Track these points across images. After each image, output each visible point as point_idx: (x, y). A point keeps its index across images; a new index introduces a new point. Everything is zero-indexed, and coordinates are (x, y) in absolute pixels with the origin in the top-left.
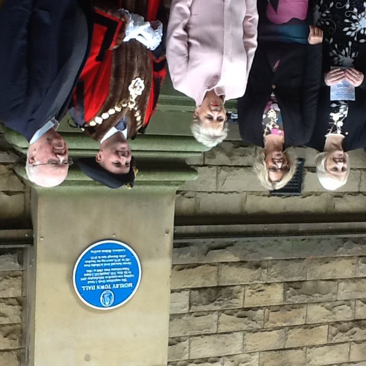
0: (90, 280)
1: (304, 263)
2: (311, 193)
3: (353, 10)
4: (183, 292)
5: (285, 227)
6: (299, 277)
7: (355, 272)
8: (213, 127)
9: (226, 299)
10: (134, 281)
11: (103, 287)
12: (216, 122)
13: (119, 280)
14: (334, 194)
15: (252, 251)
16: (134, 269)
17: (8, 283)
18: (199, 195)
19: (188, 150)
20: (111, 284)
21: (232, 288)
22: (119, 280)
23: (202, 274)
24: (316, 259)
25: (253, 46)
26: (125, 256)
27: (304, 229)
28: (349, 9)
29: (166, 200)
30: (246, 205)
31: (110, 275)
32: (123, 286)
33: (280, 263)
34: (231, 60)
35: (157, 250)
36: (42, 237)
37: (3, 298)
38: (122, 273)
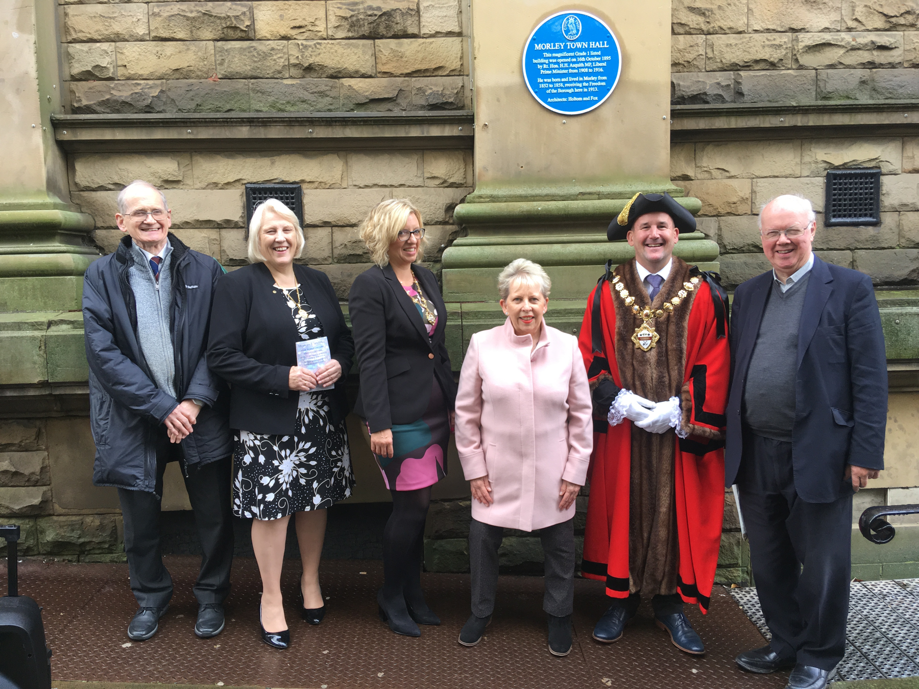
0: (598, 56)
1: (221, 71)
2: (226, 187)
3: (307, 482)
4: (433, 32)
5: (274, 133)
6: (229, 46)
7: (117, 51)
8: (528, 287)
9: (362, 17)
10: (532, 53)
11: (579, 45)
12: (524, 295)
13: (554, 55)
14: (181, 187)
15: (322, 94)
16: (533, 72)
17: (686, 54)
18: (419, 182)
19: (478, 247)
20: (566, 49)
21: (350, 34)
22: (554, 55)
23: (404, 59)
24: (198, 77)
25: (465, 408)
26: (548, 91)
27: (240, 128)
28: (313, 481)
29: (490, 174)
30: (341, 169)
31: (569, 63)
32: (548, 46)
33: (270, 72)
34: (520, 387)
35: (498, 100)
36: (664, 119)
37: (690, 34)
38: (552, 66)
